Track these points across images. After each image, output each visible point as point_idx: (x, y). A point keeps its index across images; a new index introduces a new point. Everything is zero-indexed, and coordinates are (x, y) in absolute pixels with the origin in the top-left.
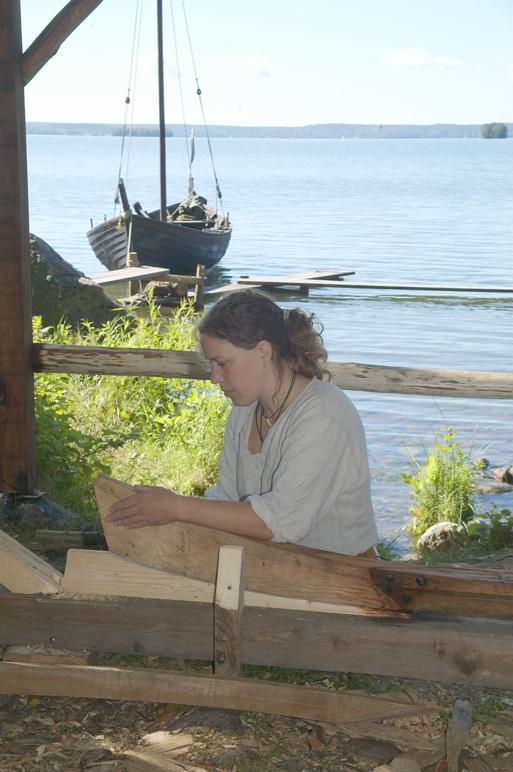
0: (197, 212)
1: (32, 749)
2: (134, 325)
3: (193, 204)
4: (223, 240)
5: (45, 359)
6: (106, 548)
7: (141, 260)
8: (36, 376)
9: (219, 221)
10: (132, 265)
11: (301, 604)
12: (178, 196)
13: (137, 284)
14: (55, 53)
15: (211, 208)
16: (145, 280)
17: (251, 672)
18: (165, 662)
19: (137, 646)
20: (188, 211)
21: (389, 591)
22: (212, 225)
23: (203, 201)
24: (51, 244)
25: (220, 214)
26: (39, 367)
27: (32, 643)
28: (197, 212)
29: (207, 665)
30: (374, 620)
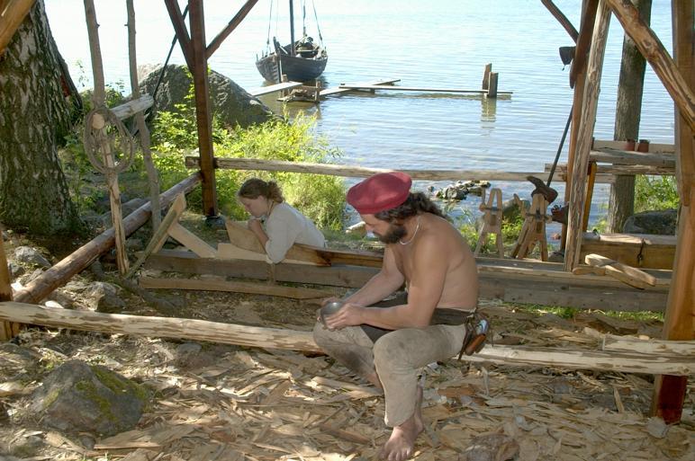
0: (308, 45)
1: (206, 306)
2: (275, 124)
3: (306, 41)
4: (322, 63)
5: (219, 164)
6: (230, 242)
7: (290, 79)
8: (12, 285)
9: (320, 51)
10: (285, 81)
11: (295, 262)
12: (299, 37)
13: (286, 92)
14: (135, 33)
15: (316, 42)
16: (291, 89)
17: (280, 283)
18: (251, 280)
19: (242, 275)
20: (304, 45)
21: (323, 257)
22: (316, 53)
23: (311, 39)
24: (236, 82)
25: (321, 46)
26: (216, 167)
27: (209, 273)
28: (308, 45)
29: (263, 281)
30: (318, 266)
